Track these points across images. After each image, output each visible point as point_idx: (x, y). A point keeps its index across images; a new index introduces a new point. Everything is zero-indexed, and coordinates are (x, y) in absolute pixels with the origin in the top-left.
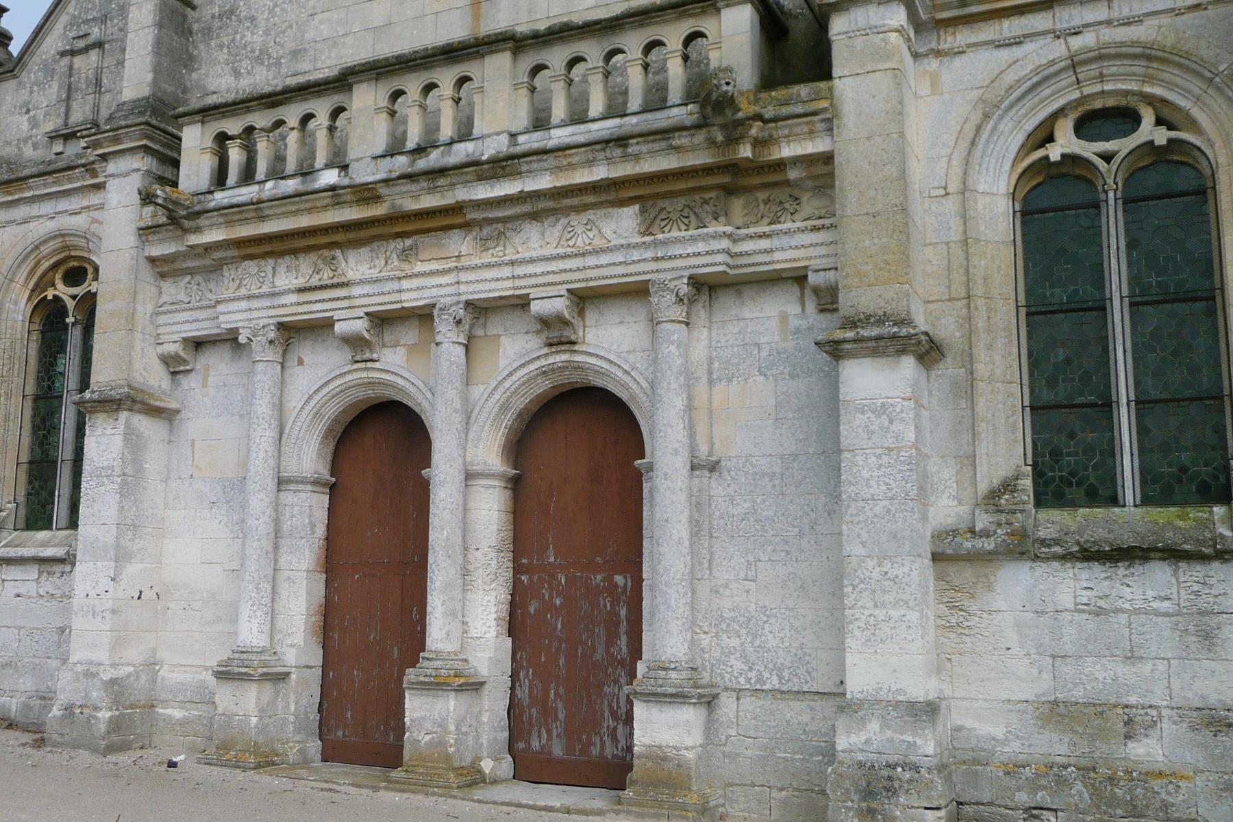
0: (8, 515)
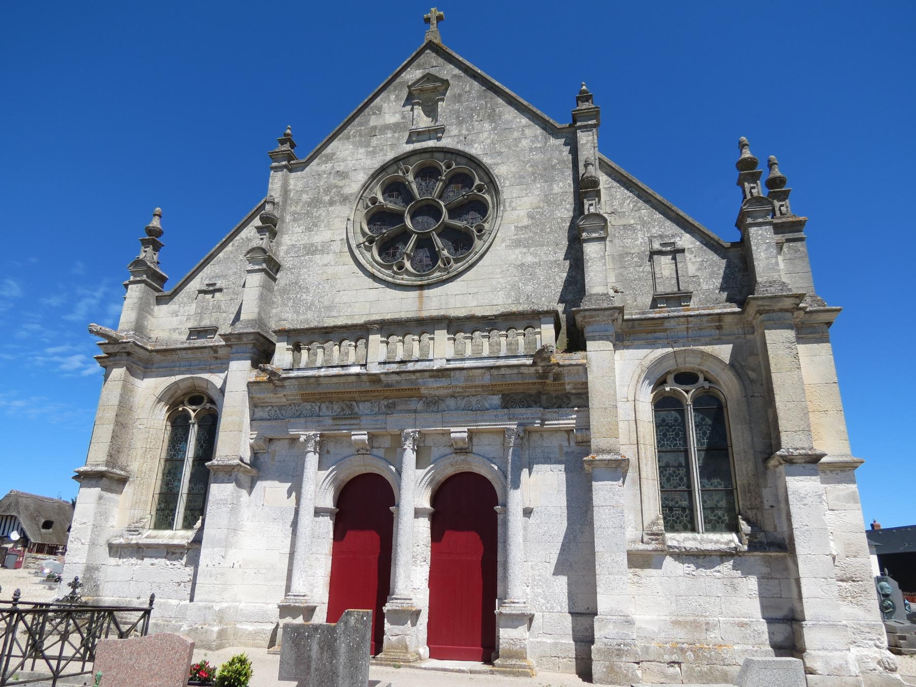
0: (147, 521)
